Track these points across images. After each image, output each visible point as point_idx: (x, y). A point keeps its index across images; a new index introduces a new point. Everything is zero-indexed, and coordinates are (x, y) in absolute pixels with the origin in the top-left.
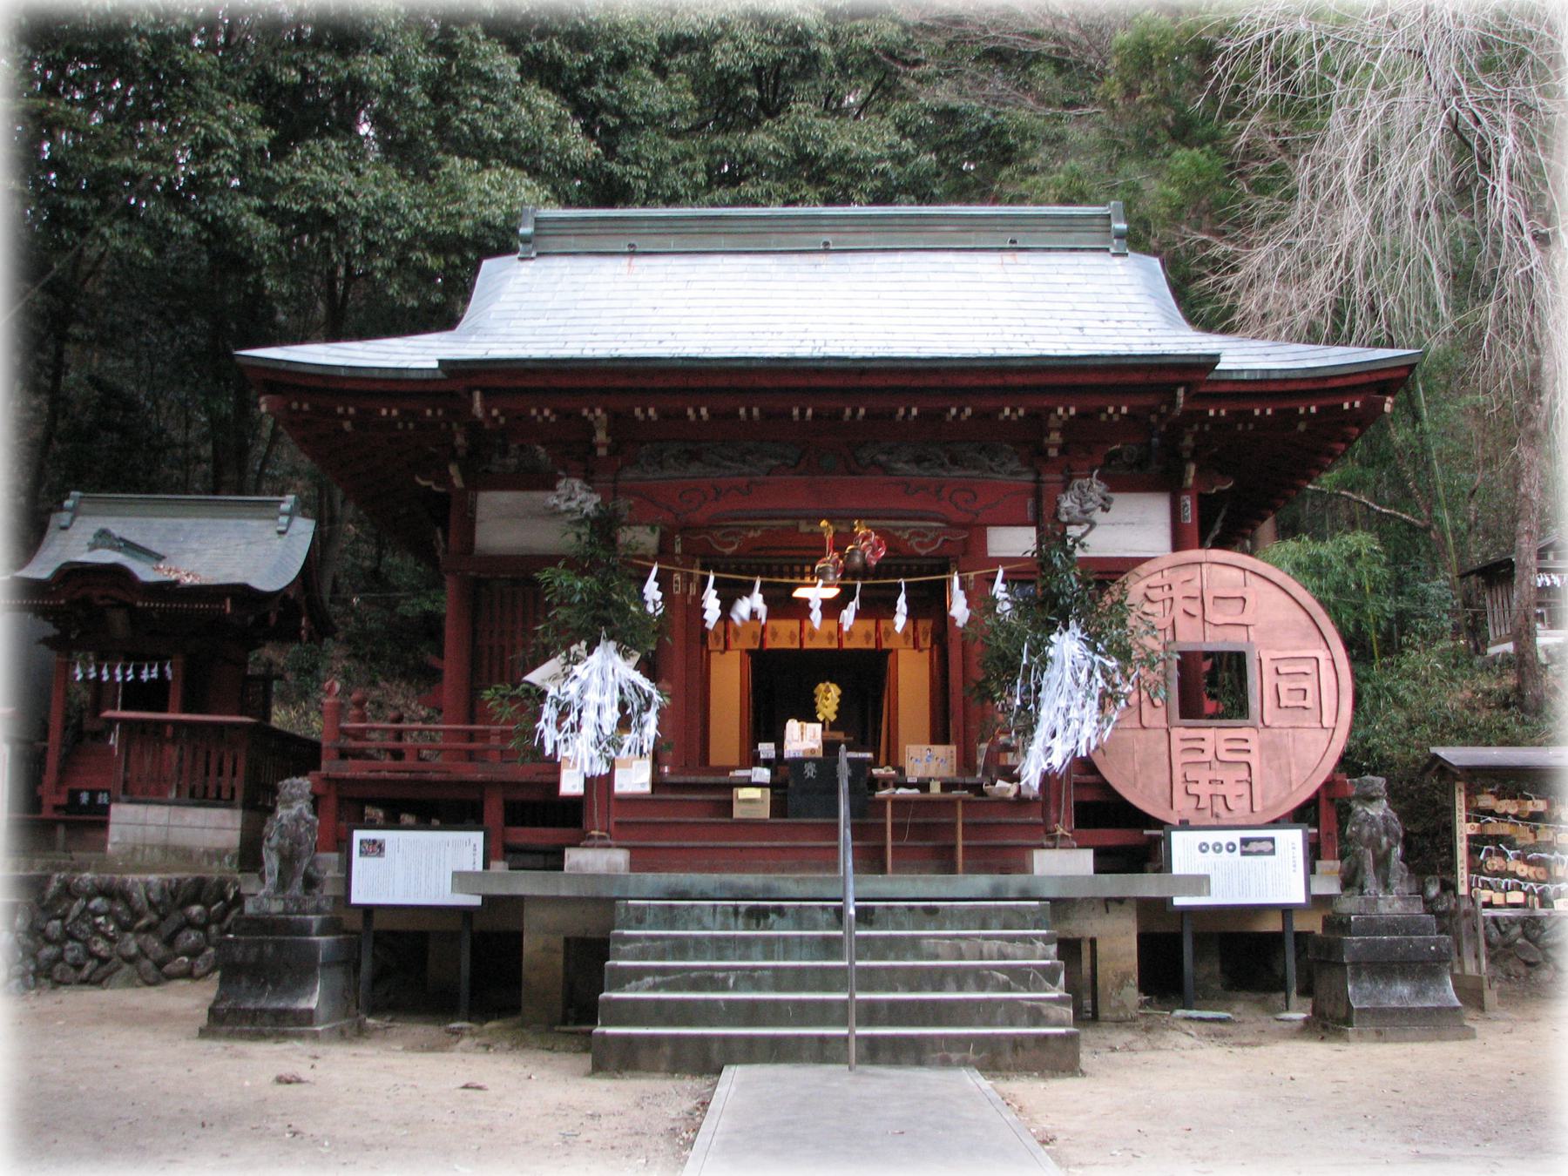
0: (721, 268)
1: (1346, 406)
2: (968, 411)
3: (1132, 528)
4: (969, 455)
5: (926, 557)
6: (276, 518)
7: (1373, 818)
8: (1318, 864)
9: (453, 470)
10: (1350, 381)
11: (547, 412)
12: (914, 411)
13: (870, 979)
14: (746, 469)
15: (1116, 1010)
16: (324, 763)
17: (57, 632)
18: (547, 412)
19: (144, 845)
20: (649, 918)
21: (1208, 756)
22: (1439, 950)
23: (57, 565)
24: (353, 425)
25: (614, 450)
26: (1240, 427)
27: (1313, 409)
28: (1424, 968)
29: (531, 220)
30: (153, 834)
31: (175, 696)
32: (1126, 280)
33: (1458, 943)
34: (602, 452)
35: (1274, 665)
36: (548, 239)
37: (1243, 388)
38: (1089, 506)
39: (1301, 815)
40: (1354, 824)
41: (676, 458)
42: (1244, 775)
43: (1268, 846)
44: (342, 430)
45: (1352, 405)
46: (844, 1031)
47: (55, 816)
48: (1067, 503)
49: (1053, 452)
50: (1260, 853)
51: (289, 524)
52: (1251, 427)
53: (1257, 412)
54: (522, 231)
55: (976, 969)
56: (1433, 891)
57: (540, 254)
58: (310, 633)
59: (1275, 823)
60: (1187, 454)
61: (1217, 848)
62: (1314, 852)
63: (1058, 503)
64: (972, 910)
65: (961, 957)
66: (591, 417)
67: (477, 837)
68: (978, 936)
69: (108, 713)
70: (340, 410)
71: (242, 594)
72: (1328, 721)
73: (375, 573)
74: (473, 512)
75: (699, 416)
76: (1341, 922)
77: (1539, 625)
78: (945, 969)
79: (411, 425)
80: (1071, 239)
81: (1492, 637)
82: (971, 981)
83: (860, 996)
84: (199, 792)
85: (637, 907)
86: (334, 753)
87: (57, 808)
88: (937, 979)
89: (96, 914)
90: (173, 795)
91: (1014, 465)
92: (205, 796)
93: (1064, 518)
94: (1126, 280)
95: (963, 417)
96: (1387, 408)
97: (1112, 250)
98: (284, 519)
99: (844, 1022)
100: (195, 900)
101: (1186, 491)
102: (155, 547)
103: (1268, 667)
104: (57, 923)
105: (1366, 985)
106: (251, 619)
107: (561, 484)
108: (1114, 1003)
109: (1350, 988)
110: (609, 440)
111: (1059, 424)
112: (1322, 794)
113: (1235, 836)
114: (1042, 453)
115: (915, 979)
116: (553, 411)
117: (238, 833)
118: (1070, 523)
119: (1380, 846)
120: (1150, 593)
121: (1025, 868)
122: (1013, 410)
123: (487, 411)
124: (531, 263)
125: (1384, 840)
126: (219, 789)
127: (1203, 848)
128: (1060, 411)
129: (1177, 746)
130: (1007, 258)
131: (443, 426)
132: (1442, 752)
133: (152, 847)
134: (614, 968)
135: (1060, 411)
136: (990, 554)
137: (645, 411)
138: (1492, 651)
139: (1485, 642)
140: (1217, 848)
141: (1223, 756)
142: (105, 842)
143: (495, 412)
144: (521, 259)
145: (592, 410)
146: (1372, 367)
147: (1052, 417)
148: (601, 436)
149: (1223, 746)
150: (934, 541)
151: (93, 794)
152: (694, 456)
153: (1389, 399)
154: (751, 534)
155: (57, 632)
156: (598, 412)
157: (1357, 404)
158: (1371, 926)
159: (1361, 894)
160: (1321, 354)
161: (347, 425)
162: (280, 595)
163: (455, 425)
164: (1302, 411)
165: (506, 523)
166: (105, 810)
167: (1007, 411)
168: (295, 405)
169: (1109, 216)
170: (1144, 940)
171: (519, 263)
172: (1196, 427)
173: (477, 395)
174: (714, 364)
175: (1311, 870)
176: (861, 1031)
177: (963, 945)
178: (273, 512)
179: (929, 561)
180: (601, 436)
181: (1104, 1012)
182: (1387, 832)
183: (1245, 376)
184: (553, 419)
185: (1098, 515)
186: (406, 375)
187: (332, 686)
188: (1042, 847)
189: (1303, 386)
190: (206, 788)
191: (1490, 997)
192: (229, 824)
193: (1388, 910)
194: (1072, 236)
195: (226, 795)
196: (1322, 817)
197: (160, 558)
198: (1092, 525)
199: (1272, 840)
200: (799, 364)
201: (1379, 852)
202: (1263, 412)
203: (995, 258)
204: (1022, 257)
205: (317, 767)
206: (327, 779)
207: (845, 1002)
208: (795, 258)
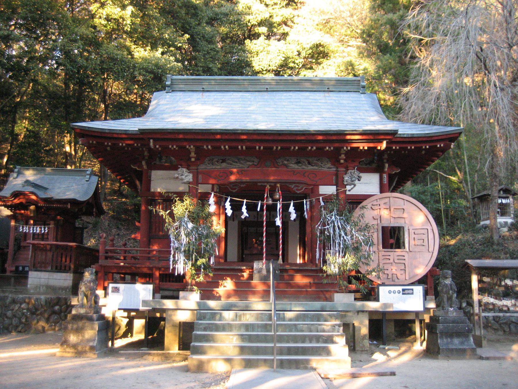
0: (232, 97)
1: (438, 146)
2: (315, 148)
3: (368, 184)
4: (315, 161)
5: (299, 194)
6: (85, 176)
7: (447, 284)
8: (427, 297)
9: (144, 163)
10: (440, 138)
11: (175, 147)
12: (297, 148)
13: (281, 339)
14: (241, 165)
15: (362, 347)
16: (100, 261)
17: (12, 213)
18: (175, 147)
19: (40, 285)
20: (208, 317)
21: (391, 261)
22: (469, 329)
23: (13, 191)
24: (111, 148)
25: (197, 159)
26: (403, 152)
27: (428, 147)
28: (463, 334)
29: (170, 79)
30: (43, 281)
31: (51, 236)
32: (365, 102)
33: (474, 326)
34: (193, 160)
35: (413, 231)
36: (174, 86)
37: (405, 140)
38: (353, 179)
39: (421, 281)
40: (441, 286)
41: (217, 162)
42: (403, 268)
43: (411, 291)
44: (107, 150)
45: (440, 145)
46: (272, 358)
47: (11, 274)
48: (346, 178)
49: (342, 161)
50: (408, 294)
51: (89, 178)
52: (407, 152)
53: (409, 148)
54: (167, 83)
55: (316, 336)
56: (464, 305)
57: (173, 91)
58: (96, 213)
59: (413, 284)
60: (385, 161)
61: (394, 292)
62: (426, 293)
63: (343, 178)
64: (314, 315)
65: (311, 331)
66: (189, 148)
67: (150, 287)
68: (316, 324)
69: (28, 241)
70: (106, 144)
71: (74, 202)
72: (431, 249)
73: (119, 190)
74: (150, 177)
75: (225, 148)
76: (436, 319)
77: (498, 215)
78: (305, 336)
79: (130, 149)
80: (347, 88)
81: (482, 219)
82: (314, 340)
83: (278, 345)
84: (59, 268)
85: (203, 313)
86: (103, 257)
87: (11, 272)
88: (303, 339)
89: (23, 309)
90: (50, 268)
91: (329, 165)
92: (61, 269)
93: (345, 183)
94: (365, 102)
95: (313, 150)
96: (452, 146)
97: (361, 92)
98: (88, 176)
99: (272, 354)
100: (57, 304)
101: (385, 172)
102: (45, 186)
103: (412, 232)
104: (10, 312)
105: (445, 340)
106: (76, 210)
107: (180, 170)
108: (361, 345)
109: (439, 341)
110: (195, 156)
111: (344, 152)
112: (429, 276)
113: (400, 288)
114: (338, 161)
115: (295, 339)
116: (177, 146)
117: (71, 281)
118: (347, 185)
119: (449, 294)
120: (373, 207)
121: (331, 299)
122: (330, 147)
123: (155, 146)
124: (170, 94)
125: (451, 292)
126: (65, 266)
127: (390, 292)
128: (345, 148)
129: (381, 258)
130: (327, 94)
131: (141, 149)
132: (469, 261)
133: (43, 286)
134: (196, 335)
135: (345, 148)
136: (320, 193)
137: (207, 146)
138: (482, 223)
139: (480, 219)
140: (394, 292)
141: (396, 261)
142: (26, 284)
143: (157, 146)
144: (167, 92)
145: (190, 146)
146: (448, 133)
147: (342, 150)
148: (193, 154)
149: (396, 258)
150: (302, 189)
151: (24, 267)
152: (224, 161)
153: (453, 144)
154: (242, 186)
155: (12, 213)
156: (192, 147)
157: (442, 145)
158: (446, 322)
159: (443, 309)
160: (430, 128)
161: (108, 148)
162: (87, 202)
163: (144, 149)
164: (424, 147)
165: (161, 182)
166: (27, 272)
167: (327, 148)
168: (91, 142)
169: (359, 81)
170: (371, 321)
171: (165, 94)
172: (389, 152)
173: (151, 141)
174: (231, 131)
175: (425, 299)
176: (278, 358)
177: (312, 327)
178: (84, 174)
179: (300, 195)
180: (193, 154)
181: (357, 348)
182: (451, 289)
183: (405, 136)
184: (177, 149)
185: (357, 182)
186: (128, 132)
187: (103, 235)
188: (337, 292)
189: (424, 139)
190: (61, 266)
191: (484, 343)
192: (68, 278)
193: (452, 315)
194: (348, 87)
195: (67, 268)
196: (430, 283)
197: (46, 189)
198: (355, 185)
199: (412, 290)
200: (259, 132)
201: (449, 296)
202: (411, 147)
203: (322, 94)
204: (331, 94)
205: (98, 262)
206: (101, 266)
207: (273, 347)
208: (257, 93)
